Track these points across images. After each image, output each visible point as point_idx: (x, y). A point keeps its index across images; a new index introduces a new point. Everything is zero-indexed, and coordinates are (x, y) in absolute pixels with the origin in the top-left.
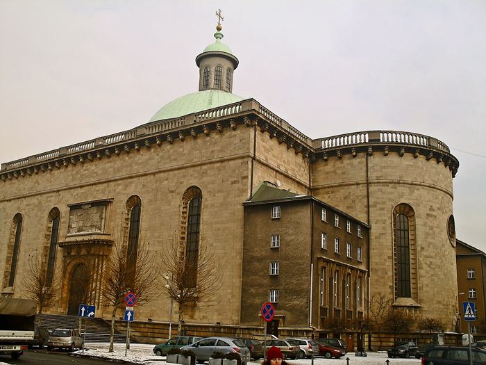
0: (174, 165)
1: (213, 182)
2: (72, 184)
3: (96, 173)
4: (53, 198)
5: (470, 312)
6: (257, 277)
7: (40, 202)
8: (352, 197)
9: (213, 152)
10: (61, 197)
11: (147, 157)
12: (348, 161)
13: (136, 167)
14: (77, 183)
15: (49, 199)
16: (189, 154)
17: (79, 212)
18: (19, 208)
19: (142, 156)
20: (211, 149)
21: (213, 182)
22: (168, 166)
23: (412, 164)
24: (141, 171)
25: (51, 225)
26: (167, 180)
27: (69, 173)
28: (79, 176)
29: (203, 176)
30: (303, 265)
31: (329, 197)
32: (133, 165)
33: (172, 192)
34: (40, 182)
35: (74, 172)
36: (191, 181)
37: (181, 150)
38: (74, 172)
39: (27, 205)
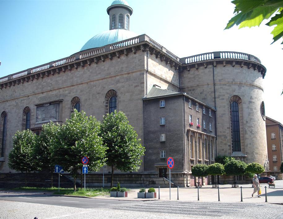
0: (99, 77)
1: (123, 87)
2: (36, 91)
3: (51, 84)
4: (25, 101)
6: (152, 143)
7: (17, 103)
8: (205, 93)
9: (122, 68)
10: (30, 100)
11: (82, 73)
12: (202, 71)
13: (76, 79)
15: (23, 101)
16: (108, 70)
17: (42, 109)
18: (4, 108)
19: (79, 72)
20: (121, 67)
21: (123, 87)
22: (96, 78)
23: (239, 71)
24: (79, 82)
25: (25, 117)
26: (95, 86)
27: (34, 85)
28: (40, 86)
29: (117, 84)
30: (179, 134)
31: (191, 93)
32: (74, 78)
33: (99, 93)
34: (16, 91)
35: (37, 84)
36: (110, 87)
37: (103, 67)
38: (37, 84)
39: (9, 106)
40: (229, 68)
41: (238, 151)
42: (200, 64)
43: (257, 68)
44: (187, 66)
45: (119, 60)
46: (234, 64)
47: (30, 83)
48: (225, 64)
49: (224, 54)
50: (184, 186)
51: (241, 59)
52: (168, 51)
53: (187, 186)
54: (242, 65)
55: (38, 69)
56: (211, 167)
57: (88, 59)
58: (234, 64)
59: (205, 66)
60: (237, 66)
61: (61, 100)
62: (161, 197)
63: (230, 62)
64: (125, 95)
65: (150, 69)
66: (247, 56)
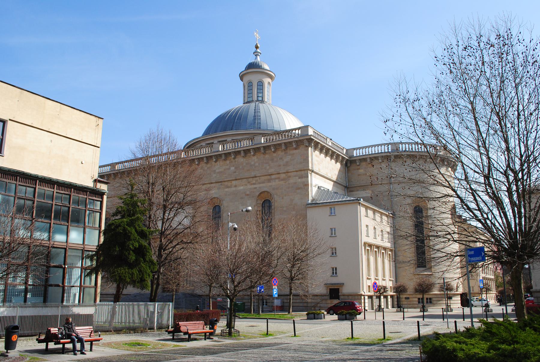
42: (372, 159)
45: (275, 155)
57: (233, 152)
64: (283, 198)
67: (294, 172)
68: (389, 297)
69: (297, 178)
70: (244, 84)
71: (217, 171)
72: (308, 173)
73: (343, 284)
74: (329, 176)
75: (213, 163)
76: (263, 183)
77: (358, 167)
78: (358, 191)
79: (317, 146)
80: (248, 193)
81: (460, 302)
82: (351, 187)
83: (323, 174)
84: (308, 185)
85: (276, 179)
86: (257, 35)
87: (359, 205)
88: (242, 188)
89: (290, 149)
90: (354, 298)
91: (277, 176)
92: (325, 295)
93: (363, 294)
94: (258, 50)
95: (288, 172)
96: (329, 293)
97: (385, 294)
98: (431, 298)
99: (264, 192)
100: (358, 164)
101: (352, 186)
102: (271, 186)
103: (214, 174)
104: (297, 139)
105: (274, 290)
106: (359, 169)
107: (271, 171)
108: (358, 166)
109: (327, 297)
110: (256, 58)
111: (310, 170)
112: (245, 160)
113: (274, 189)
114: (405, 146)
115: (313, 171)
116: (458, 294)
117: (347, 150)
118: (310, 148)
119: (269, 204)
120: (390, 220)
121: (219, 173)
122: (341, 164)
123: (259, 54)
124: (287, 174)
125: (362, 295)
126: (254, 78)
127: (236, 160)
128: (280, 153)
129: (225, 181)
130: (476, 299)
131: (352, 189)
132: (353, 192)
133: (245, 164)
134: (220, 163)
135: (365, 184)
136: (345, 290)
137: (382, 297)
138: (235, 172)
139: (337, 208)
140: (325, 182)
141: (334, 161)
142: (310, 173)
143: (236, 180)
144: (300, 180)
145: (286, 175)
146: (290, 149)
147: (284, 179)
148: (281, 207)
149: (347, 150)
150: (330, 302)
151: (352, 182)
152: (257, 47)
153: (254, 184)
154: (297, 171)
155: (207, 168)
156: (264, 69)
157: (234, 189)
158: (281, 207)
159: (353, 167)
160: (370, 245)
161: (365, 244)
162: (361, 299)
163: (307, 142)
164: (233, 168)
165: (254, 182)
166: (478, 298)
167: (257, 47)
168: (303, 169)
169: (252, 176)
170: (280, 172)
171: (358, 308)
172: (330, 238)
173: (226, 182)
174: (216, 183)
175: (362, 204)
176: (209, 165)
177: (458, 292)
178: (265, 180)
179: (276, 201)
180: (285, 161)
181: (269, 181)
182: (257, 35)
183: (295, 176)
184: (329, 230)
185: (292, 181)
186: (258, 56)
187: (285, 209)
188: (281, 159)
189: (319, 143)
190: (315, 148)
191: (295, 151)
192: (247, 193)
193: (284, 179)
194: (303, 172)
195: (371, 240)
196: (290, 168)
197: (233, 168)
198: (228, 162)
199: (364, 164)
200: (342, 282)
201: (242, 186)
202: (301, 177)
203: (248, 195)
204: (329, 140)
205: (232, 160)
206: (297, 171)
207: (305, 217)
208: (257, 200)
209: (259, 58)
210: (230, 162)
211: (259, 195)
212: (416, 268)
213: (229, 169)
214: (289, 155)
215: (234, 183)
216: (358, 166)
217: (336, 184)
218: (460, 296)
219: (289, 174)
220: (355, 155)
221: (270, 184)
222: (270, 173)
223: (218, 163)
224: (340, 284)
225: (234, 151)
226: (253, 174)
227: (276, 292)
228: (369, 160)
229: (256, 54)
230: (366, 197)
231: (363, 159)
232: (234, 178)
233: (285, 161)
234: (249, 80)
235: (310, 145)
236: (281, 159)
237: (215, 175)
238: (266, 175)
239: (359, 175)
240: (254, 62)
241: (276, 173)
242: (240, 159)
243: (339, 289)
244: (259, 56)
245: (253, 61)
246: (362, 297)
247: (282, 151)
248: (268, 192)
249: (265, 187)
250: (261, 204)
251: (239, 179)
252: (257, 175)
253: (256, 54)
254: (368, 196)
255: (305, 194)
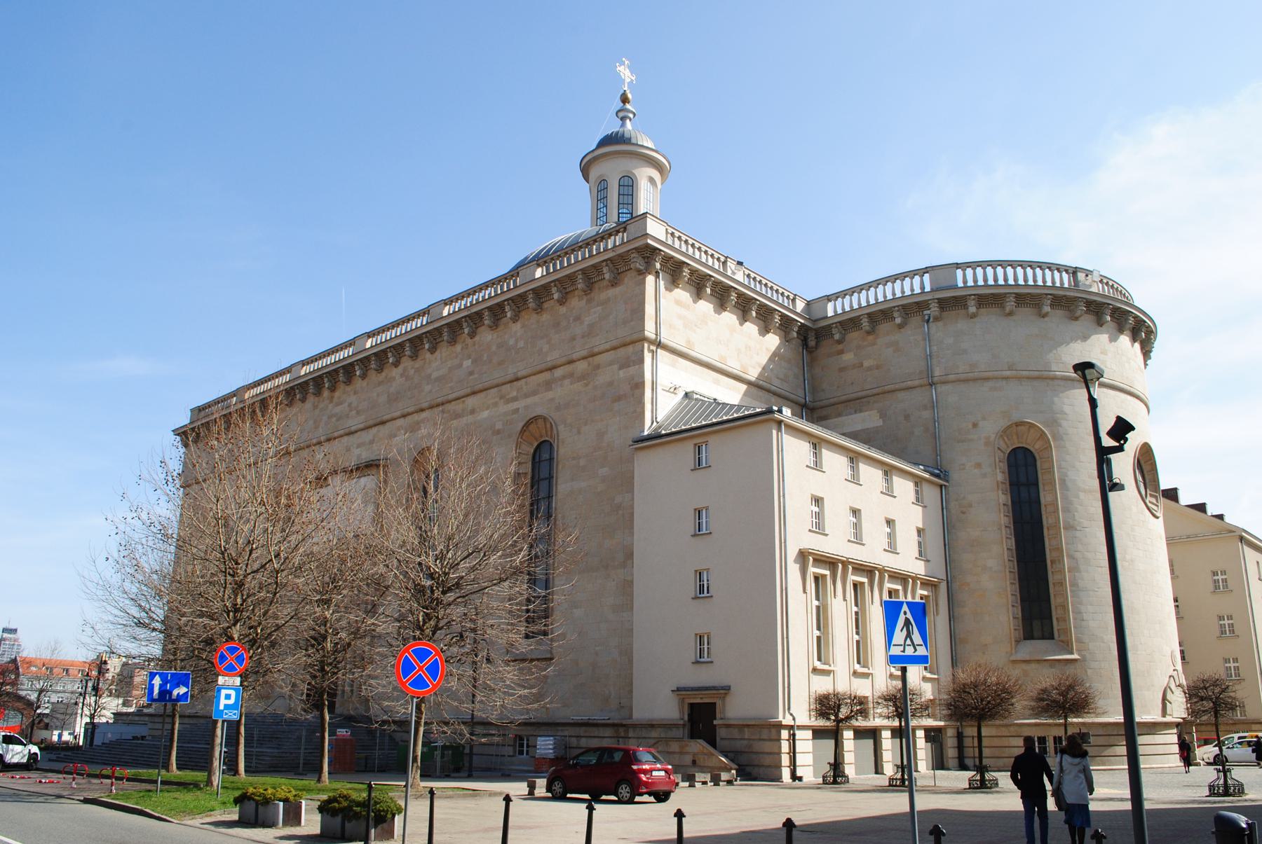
5: (909, 635)
14: (321, 434)
40: (990, 320)
41: (1043, 638)
42: (879, 316)
43: (1109, 318)
44: (829, 326)
45: (563, 310)
46: (1010, 304)
47: (295, 410)
48: (972, 309)
49: (979, 271)
50: (778, 778)
51: (1003, 283)
52: (1105, 281)
53: (794, 777)
54: (1047, 309)
55: (332, 359)
56: (421, 725)
57: (465, 317)
58: (1010, 304)
59: (898, 321)
60: (1026, 312)
61: (375, 463)
62: (408, 835)
63: (991, 300)
64: (579, 432)
65: (665, 338)
66: (1065, 276)
67: (607, 351)
68: (886, 734)
69: (616, 367)
70: (590, 187)
71: (435, 375)
72: (643, 351)
73: (728, 688)
74: (734, 366)
75: (428, 355)
76: (534, 393)
77: (840, 347)
78: (839, 415)
79: (675, 271)
80: (499, 426)
81: (1176, 749)
82: (822, 407)
83: (735, 372)
84: (643, 384)
85: (564, 377)
86: (625, 73)
87: (779, 430)
88: (485, 414)
89: (599, 289)
90: (757, 737)
91: (568, 368)
92: (676, 726)
93: (787, 721)
94: (628, 106)
95: (593, 355)
96: (686, 717)
97: (860, 723)
98: (1044, 738)
99: (536, 418)
100: (837, 337)
101: (821, 404)
102: (552, 400)
103: (428, 384)
104: (610, 255)
105: (224, 692)
106: (841, 352)
107: (554, 357)
108: (839, 342)
109: (678, 733)
110: (623, 125)
111: (651, 342)
112: (495, 335)
113: (558, 408)
114: (975, 274)
115: (659, 345)
116: (1167, 725)
117: (809, 304)
118: (650, 279)
119: (550, 456)
120: (931, 494)
121: (439, 379)
122: (786, 339)
123: (631, 116)
124: (591, 359)
125: (780, 726)
126: (611, 170)
127: (477, 338)
128: (576, 303)
129: (450, 402)
130: (1239, 738)
131: (824, 412)
132: (828, 421)
133: (494, 348)
134: (444, 351)
135: (860, 394)
136: (735, 709)
137: (848, 735)
138: (471, 373)
139: (714, 441)
140: (717, 382)
141: (734, 317)
142: (650, 351)
143: (474, 393)
144: (622, 373)
145: (589, 365)
146: (599, 289)
147: (583, 377)
148: (574, 459)
149: (809, 304)
150: (677, 750)
151: (823, 390)
152: (625, 99)
153: (515, 399)
154: (614, 348)
155: (415, 372)
156: (637, 145)
157: (470, 419)
158: (574, 459)
159: (826, 347)
160: (831, 563)
161: (803, 556)
162: (779, 739)
163: (640, 260)
164: (467, 363)
165: (515, 394)
166: (1245, 737)
167: (625, 99)
168: (628, 339)
169: (509, 378)
170: (575, 356)
171: (643, 777)
172: (693, 540)
173: (453, 403)
174: (431, 407)
175: (788, 426)
176: (418, 363)
177: (1168, 719)
178: (539, 385)
179: (563, 442)
180: (586, 323)
181: (548, 385)
182: (625, 73)
183: (611, 364)
184: (691, 515)
185: (603, 378)
186: (628, 121)
187: (582, 462)
188: (578, 318)
189: (684, 263)
190: (674, 281)
191: (612, 292)
192: (497, 427)
193: (583, 377)
194: (630, 349)
195: (836, 544)
196: (599, 342)
197: (467, 363)
198: (458, 347)
199: (854, 336)
200: (725, 683)
201: (487, 409)
202: (625, 364)
203: (498, 432)
204: (733, 267)
205: (469, 341)
206: (614, 348)
207: (626, 482)
208: (518, 445)
209: (628, 124)
210: (462, 349)
211: (523, 431)
212: (1017, 642)
213: (460, 365)
214: (598, 305)
215: (471, 402)
216: (839, 342)
217: (754, 390)
218: (1175, 731)
219: (597, 359)
220: (830, 313)
221: (550, 395)
222: (550, 365)
223: (437, 353)
224: (723, 688)
225: (466, 313)
226: (511, 371)
227: (232, 701)
228: (865, 323)
229: (621, 114)
230: (863, 430)
231: (850, 323)
232: (469, 390)
233: (586, 323)
234: (598, 177)
235: (648, 269)
236: (578, 318)
237: (427, 388)
238: (541, 372)
239: (842, 370)
240: (617, 133)
241: (563, 360)
242: (486, 336)
243: (714, 704)
244: (630, 120)
245: (616, 130)
246: (785, 734)
247: (580, 298)
248: (545, 419)
249: (537, 404)
250: (530, 457)
251: (481, 391)
252: (520, 374)
253: (621, 114)
254: (868, 429)
255: (635, 411)
